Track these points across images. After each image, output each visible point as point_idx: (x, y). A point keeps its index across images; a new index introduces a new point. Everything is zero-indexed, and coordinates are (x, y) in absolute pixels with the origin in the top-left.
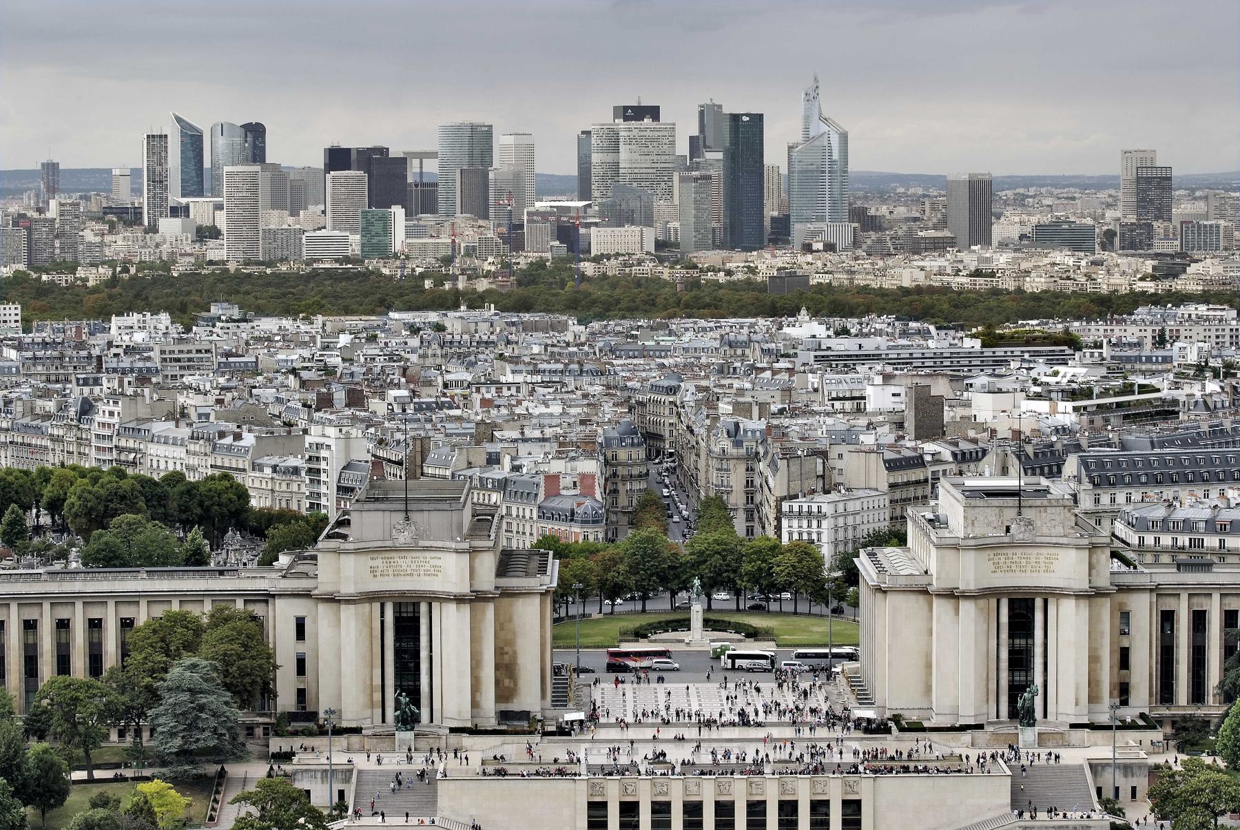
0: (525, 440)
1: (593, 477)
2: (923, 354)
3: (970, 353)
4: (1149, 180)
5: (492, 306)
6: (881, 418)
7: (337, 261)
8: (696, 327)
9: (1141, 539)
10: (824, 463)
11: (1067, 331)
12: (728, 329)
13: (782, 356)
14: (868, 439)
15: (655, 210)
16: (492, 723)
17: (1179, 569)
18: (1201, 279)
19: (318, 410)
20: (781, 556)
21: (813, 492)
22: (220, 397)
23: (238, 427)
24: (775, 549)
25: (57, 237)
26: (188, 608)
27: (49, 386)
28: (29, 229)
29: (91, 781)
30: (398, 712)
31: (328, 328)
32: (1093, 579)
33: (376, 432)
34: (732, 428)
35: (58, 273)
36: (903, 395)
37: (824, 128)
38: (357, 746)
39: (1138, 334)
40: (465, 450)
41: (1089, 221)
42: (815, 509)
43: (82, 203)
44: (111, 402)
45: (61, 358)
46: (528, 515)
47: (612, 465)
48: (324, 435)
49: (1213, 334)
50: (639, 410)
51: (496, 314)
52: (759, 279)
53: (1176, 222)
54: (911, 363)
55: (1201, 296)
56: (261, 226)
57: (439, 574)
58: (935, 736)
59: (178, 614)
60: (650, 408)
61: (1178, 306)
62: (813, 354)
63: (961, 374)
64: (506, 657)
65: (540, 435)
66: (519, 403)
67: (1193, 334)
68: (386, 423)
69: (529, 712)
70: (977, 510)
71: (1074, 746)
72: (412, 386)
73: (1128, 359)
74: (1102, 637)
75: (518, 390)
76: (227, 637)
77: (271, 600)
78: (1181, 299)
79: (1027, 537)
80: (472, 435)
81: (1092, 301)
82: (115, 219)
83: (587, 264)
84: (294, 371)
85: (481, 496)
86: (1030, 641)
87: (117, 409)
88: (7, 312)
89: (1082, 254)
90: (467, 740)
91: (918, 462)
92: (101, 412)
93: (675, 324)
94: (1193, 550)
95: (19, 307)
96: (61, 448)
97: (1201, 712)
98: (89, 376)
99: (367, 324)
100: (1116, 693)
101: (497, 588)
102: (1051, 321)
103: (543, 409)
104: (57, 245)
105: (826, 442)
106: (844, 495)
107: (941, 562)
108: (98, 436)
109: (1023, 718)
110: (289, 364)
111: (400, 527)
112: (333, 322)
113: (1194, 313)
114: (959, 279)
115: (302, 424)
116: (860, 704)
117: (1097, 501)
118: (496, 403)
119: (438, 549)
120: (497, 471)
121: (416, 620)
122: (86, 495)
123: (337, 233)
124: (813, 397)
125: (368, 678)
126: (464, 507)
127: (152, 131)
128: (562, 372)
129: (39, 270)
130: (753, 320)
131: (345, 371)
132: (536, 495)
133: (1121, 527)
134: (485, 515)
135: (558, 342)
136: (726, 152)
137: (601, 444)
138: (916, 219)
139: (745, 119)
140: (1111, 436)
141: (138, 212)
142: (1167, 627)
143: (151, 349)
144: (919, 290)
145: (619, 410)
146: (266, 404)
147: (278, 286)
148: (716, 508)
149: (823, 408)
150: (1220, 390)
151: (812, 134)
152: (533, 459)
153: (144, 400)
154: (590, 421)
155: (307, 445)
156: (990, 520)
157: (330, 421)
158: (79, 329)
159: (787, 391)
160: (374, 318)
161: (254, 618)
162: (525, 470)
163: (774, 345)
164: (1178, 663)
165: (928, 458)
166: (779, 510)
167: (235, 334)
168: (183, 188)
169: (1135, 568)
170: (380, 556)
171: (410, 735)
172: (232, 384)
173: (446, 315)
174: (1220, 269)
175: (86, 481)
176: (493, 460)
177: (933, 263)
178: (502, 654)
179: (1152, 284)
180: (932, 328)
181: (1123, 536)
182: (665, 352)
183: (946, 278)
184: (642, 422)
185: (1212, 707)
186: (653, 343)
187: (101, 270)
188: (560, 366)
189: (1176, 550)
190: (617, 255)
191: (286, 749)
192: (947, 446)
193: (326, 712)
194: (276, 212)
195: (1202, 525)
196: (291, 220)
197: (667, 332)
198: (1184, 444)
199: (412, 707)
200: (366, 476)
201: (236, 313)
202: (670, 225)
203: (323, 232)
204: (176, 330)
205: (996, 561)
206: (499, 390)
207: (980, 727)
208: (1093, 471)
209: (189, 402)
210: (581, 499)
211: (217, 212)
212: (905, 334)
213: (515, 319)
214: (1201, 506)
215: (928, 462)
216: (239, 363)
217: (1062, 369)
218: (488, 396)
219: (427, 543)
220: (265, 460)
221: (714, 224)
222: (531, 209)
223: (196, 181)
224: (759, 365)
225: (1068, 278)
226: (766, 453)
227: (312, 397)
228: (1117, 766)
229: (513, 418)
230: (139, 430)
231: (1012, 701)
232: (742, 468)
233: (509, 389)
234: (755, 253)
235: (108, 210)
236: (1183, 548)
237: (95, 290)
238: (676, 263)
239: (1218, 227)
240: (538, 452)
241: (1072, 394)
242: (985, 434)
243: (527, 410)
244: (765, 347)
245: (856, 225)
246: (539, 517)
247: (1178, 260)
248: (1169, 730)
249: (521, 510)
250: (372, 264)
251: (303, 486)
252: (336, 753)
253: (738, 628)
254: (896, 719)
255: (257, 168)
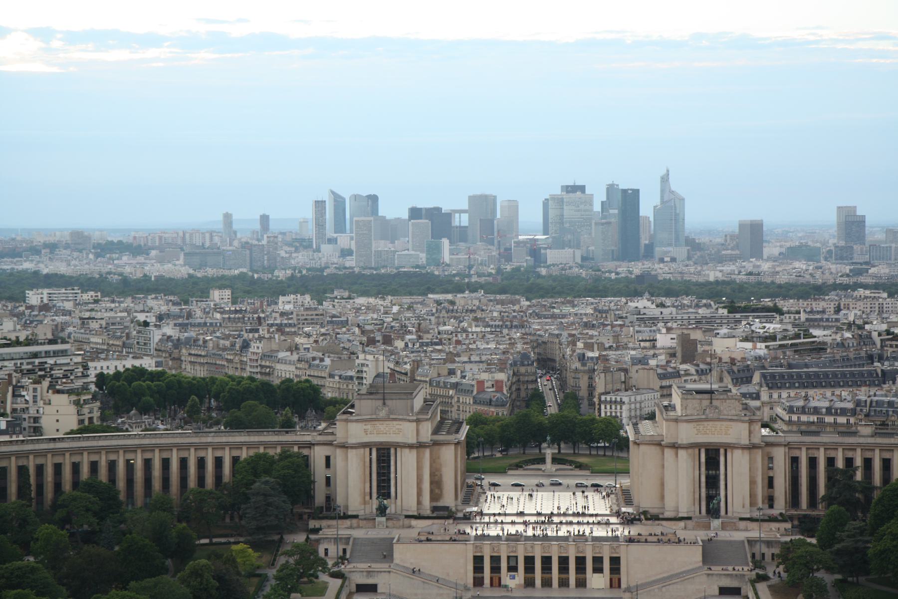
0: (471, 362)
1: (502, 382)
4: (853, 222)
6: (661, 351)
7: (413, 267)
11: (775, 305)
13: (620, 318)
16: (428, 512)
18: (874, 276)
19: (367, 346)
21: (618, 390)
24: (593, 420)
28: (251, 250)
29: (211, 544)
32: (752, 439)
34: (581, 357)
38: (355, 525)
41: (818, 245)
42: (619, 399)
45: (244, 317)
46: (468, 402)
47: (517, 376)
48: (365, 359)
49: (869, 306)
53: (867, 245)
56: (373, 249)
58: (664, 523)
66: (474, 342)
67: (857, 306)
68: (401, 353)
69: (448, 507)
70: (688, 401)
71: (742, 530)
72: (865, 333)
73: (816, 320)
77: (312, 447)
79: (716, 416)
80: (444, 359)
83: (543, 269)
84: (359, 326)
86: (718, 472)
87: (260, 345)
88: (224, 294)
89: (812, 263)
90: (414, 522)
91: (677, 374)
99: (413, 301)
100: (766, 501)
101: (431, 440)
108: (250, 360)
112: (395, 299)
117: (771, 397)
121: (389, 457)
123: (413, 252)
128: (502, 326)
130: (619, 299)
132: (472, 391)
139: (630, 192)
144: (717, 282)
145: (525, 346)
152: (474, 374)
156: (695, 403)
158: (262, 303)
165: (682, 373)
166: (600, 399)
169: (777, 433)
171: (384, 519)
174: (887, 271)
175: (235, 383)
176: (452, 372)
180: (712, 303)
181: (781, 416)
187: (287, 272)
188: (501, 323)
191: (317, 526)
195: (824, 410)
196: (390, 245)
201: (346, 294)
204: (314, 304)
206: (467, 336)
207: (689, 518)
213: (492, 298)
217: (767, 325)
218: (460, 338)
221: (613, 248)
222: (516, 240)
224: (606, 323)
225: (800, 276)
227: (365, 339)
228: (764, 542)
232: (586, 377)
236: (813, 423)
239: (891, 247)
240: (475, 367)
241: (765, 339)
248: (796, 523)
252: (343, 529)
253: (571, 463)
254: (645, 513)
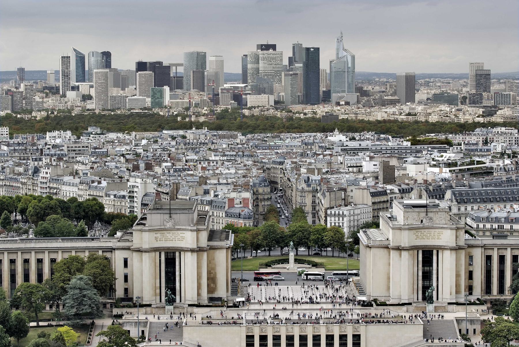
0: (220, 184)
1: (248, 199)
2: (386, 148)
3: (406, 147)
4: (481, 75)
5: (206, 128)
6: (369, 175)
7: (141, 109)
8: (291, 137)
9: (478, 225)
10: (345, 193)
11: (446, 138)
12: (305, 138)
13: (327, 149)
14: (363, 184)
15: (274, 88)
16: (206, 302)
17: (493, 238)
18: (503, 117)
19: (133, 171)
20: (327, 233)
21: (340, 206)
22: (92, 166)
23: (100, 178)
24: (324, 229)
25: (24, 99)
26: (79, 254)
27: (21, 161)
28: (12, 96)
29: (38, 326)
30: (167, 298)
31: (137, 137)
32: (458, 242)
33: (157, 180)
34: (306, 179)
35: (24, 114)
36: (378, 165)
37: (345, 54)
38: (149, 312)
39: (476, 140)
40: (195, 188)
41: (456, 92)
42: (341, 213)
43: (34, 85)
44: (46, 168)
45: (26, 150)
46: (221, 215)
47: (256, 195)
48: (135, 182)
49: (508, 140)
50: (267, 171)
51: (208, 131)
52: (318, 117)
53: (492, 93)
54: (381, 152)
55: (503, 124)
56: (109, 95)
57: (184, 240)
58: (391, 308)
59: (74, 257)
60: (272, 170)
61: (493, 128)
62: (340, 148)
63: (402, 156)
64: (212, 275)
65: (226, 182)
66: (217, 168)
67: (499, 140)
68: (162, 177)
69: (221, 298)
70: (409, 213)
71: (449, 312)
72: (172, 161)
73: (472, 150)
74: (461, 266)
75: (217, 163)
76: (95, 266)
77: (113, 251)
78: (494, 125)
79: (430, 224)
80: (197, 182)
81: (457, 126)
82: (48, 92)
83: (246, 110)
84: (123, 155)
85: (201, 207)
86: (431, 268)
87: (49, 171)
88: (3, 130)
89: (453, 106)
90: (195, 309)
91: (384, 193)
92: (42, 172)
93: (282, 136)
94: (499, 230)
95: (8, 128)
96: (26, 187)
97: (503, 298)
98: (37, 157)
99: (154, 136)
100: (467, 290)
101: (208, 246)
102: (440, 134)
103: (227, 171)
104: (24, 102)
105: (346, 185)
106: (353, 207)
107: (394, 235)
108: (41, 182)
109: (428, 300)
110: (121, 152)
111: (167, 220)
113: (500, 131)
114: (401, 117)
115: (126, 177)
116: (360, 294)
117: (459, 209)
118: (208, 168)
119: (183, 230)
120: (208, 197)
121: (174, 259)
122: (36, 207)
123: (141, 97)
124: (340, 166)
125: (154, 284)
126: (194, 212)
127: (64, 55)
128: (235, 155)
129: (16, 113)
130: (315, 134)
131: (144, 155)
132: (224, 207)
133: (469, 220)
134: (203, 215)
135: (234, 143)
136: (304, 64)
137: (251, 186)
138: (383, 92)
139: (312, 50)
140: (465, 182)
141: (58, 89)
142: (489, 262)
143: (63, 146)
144: (384, 121)
145: (259, 171)
146: (111, 169)
147: (116, 119)
148: (300, 212)
149: (344, 171)
150: (510, 163)
151: (340, 56)
152: (223, 192)
153: (60, 167)
154: (247, 176)
155: (128, 186)
156: (414, 217)
157: (138, 176)
158: (33, 137)
159: (330, 163)
160: (156, 133)
161: (106, 259)
162: (220, 197)
163: (324, 144)
164: (493, 277)
165: (388, 192)
166: (326, 213)
167: (98, 140)
168: (77, 79)
169: (475, 237)
170: (159, 233)
171: (171, 307)
172: (97, 161)
173: (187, 132)
174: (511, 113)
175: (36, 201)
176: (206, 192)
177: (391, 110)
178: (210, 273)
179: (482, 119)
180: (390, 137)
181: (470, 224)
182: (278, 147)
183: (396, 116)
184: (269, 177)
185: (507, 296)
186: (273, 143)
187: (42, 113)
188: (234, 153)
189: (492, 230)
190: (258, 107)
191: (120, 313)
192: (396, 186)
193: (137, 297)
194: (116, 89)
195: (503, 220)
196: (122, 92)
197: (279, 139)
198: (496, 186)
199: (173, 296)
200: (153, 199)
201: (99, 131)
202: (281, 94)
203: (135, 97)
204: (74, 138)
205: (417, 235)
206: (209, 163)
207: (410, 304)
208: (458, 197)
209: (79, 168)
210: (243, 209)
211: (91, 89)
212: (379, 139)
213: (215, 134)
214: (503, 212)
215: (388, 193)
216: (100, 152)
217: (444, 154)
218: (204, 166)
219: (179, 227)
220: (111, 192)
221: (299, 94)
222: (222, 87)
223: (82, 76)
224: (318, 153)
225: (447, 116)
226: (321, 189)
227: (130, 166)
228: (468, 320)
229: (215, 175)
230: (58, 180)
231: (424, 293)
232: (310, 196)
233: (213, 163)
234: (316, 106)
235: (45, 88)
236: (495, 229)
237: (40, 121)
238: (283, 110)
239: (510, 95)
240: (225, 189)
241: (449, 165)
242: (412, 182)
243: (221, 171)
244: (320, 145)
245: (358, 94)
246: (226, 216)
247: (493, 109)
248: (489, 305)
249: (218, 213)
250: (156, 110)
251: (127, 203)
252: (141, 315)
253: (309, 263)
254: (375, 300)
255: (108, 70)
